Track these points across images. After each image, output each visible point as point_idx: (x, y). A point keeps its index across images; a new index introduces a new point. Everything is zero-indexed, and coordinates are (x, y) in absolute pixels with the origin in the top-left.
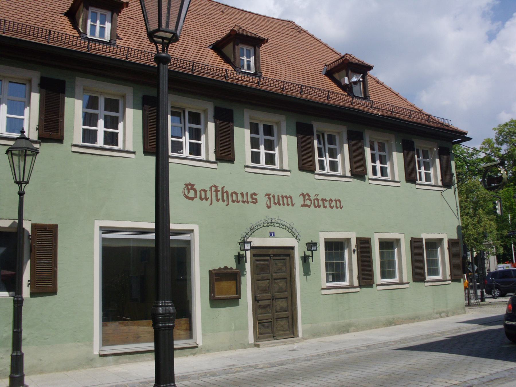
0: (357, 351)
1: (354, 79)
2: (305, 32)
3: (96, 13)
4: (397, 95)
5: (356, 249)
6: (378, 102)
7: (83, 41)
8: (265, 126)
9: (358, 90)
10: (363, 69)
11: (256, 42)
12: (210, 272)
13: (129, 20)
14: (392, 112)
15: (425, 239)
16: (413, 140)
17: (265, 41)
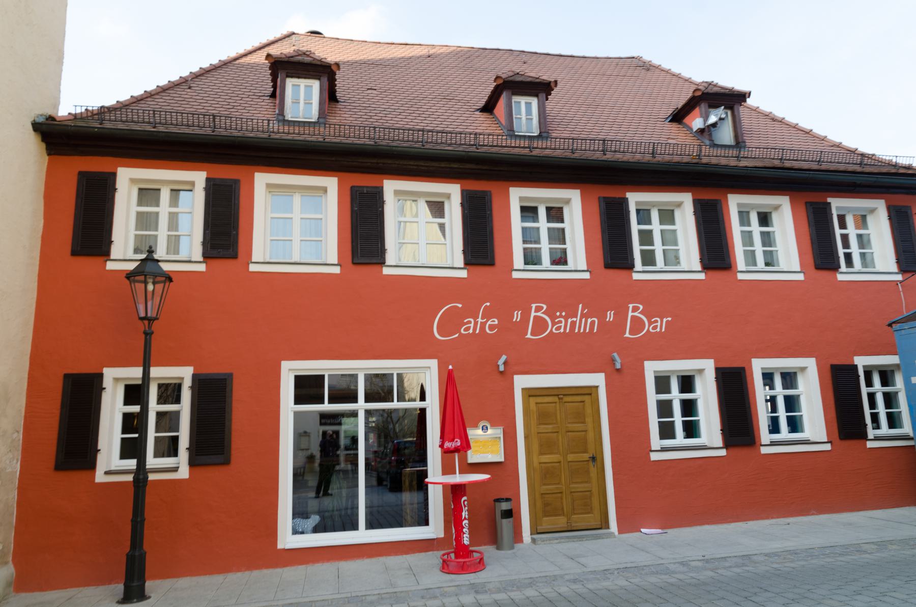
0: (682, 568)
1: (713, 119)
2: (657, 67)
3: (299, 86)
4: (808, 133)
5: (318, 454)
6: (760, 150)
7: (307, 128)
8: (759, 214)
9: (726, 135)
10: (732, 99)
11: (541, 89)
12: (227, 462)
13: (370, 91)
14: (781, 159)
15: (864, 367)
16: (829, 200)
17: (552, 85)
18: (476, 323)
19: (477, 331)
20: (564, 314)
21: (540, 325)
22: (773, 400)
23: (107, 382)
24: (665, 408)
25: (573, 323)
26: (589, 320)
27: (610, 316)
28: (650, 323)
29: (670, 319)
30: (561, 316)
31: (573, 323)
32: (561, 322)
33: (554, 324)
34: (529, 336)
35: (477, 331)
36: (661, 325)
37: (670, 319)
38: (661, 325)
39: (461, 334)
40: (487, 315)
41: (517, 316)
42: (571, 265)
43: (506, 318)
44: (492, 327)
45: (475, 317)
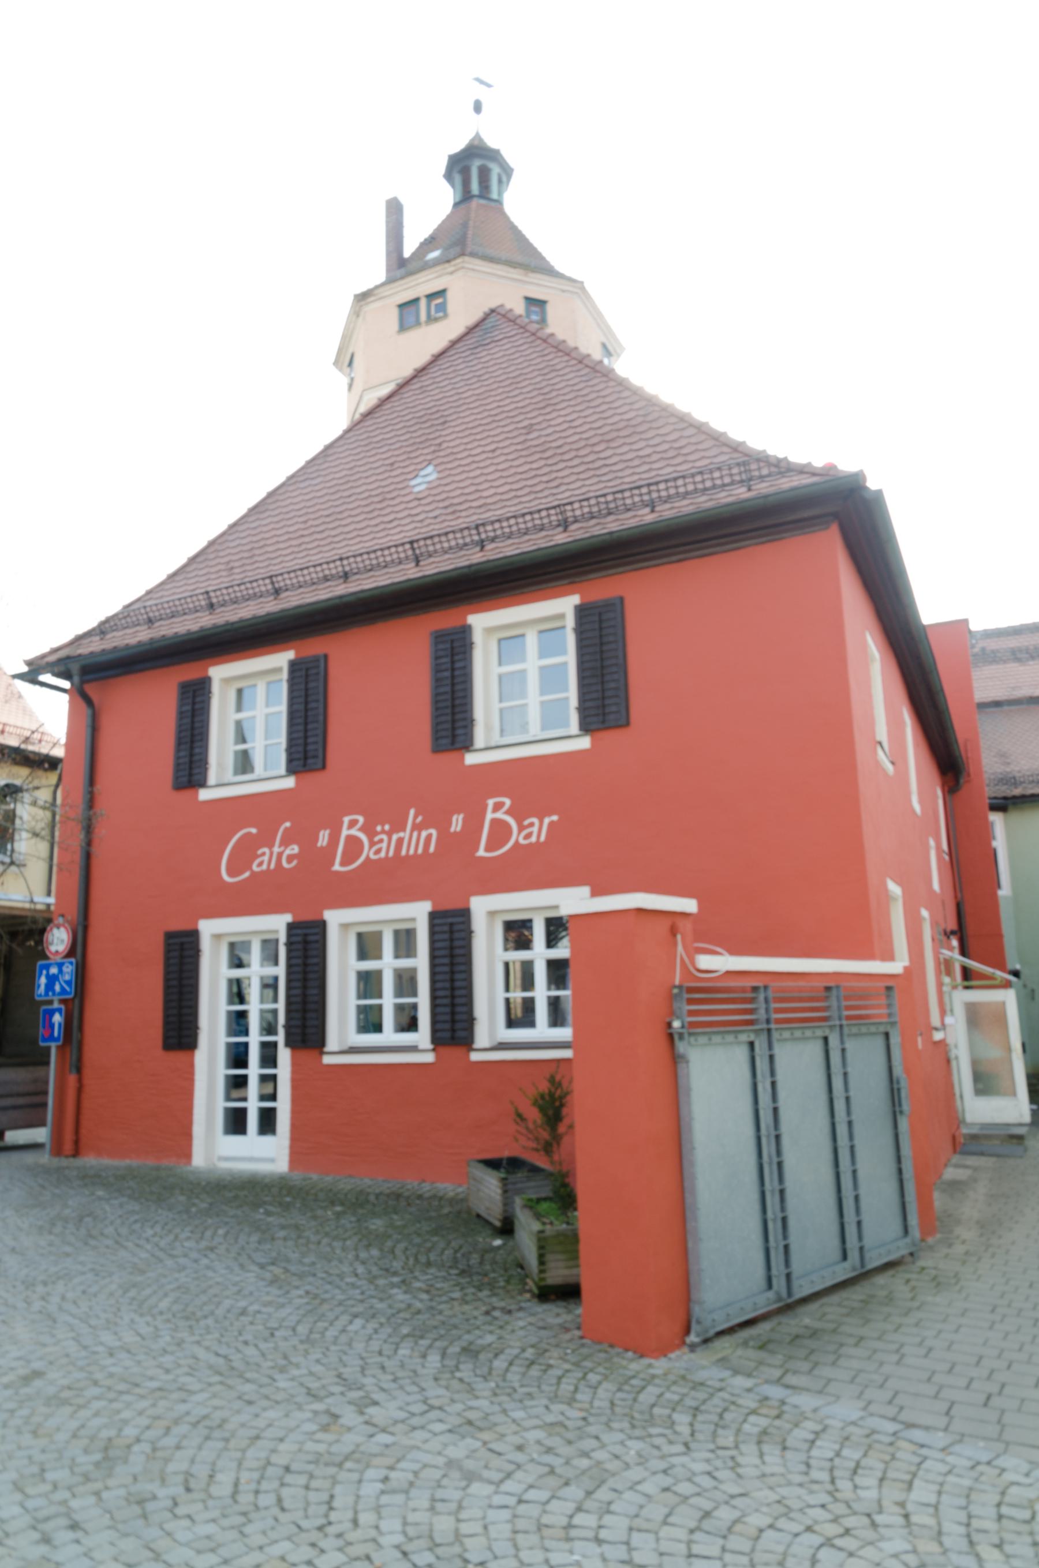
18: (271, 854)
19: (432, 849)
20: (387, 827)
21: (354, 847)
22: (238, 993)
23: (206, 944)
24: (369, 983)
25: (400, 841)
26: (424, 834)
27: (457, 823)
28: (521, 828)
29: (555, 818)
30: (383, 832)
31: (400, 841)
32: (381, 841)
33: (372, 844)
34: (481, 852)
35: (432, 849)
36: (538, 830)
37: (555, 818)
38: (538, 830)
39: (253, 873)
40: (285, 842)
41: (323, 838)
42: (259, 770)
43: (308, 841)
44: (290, 859)
45: (271, 846)
